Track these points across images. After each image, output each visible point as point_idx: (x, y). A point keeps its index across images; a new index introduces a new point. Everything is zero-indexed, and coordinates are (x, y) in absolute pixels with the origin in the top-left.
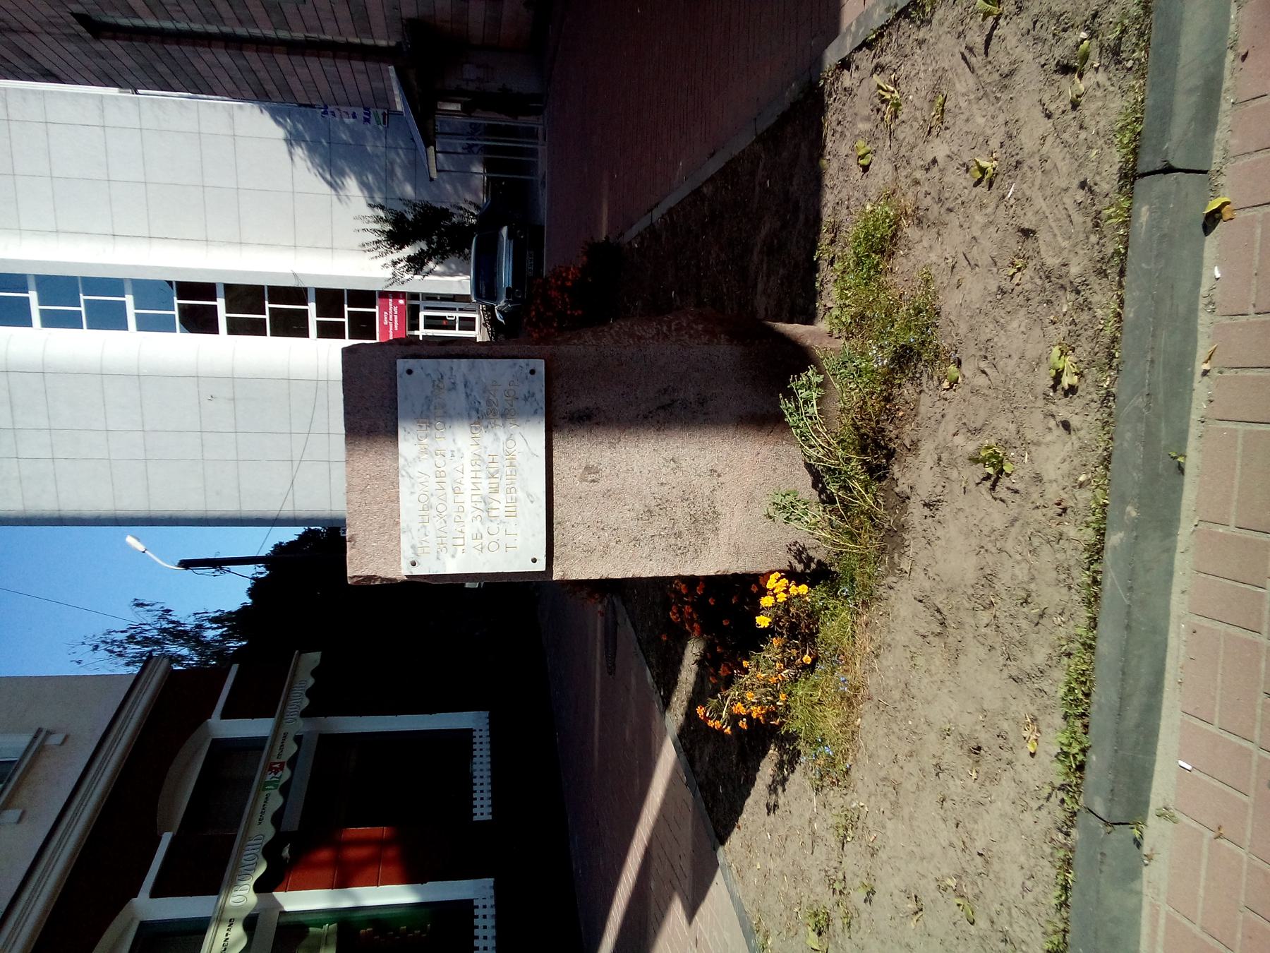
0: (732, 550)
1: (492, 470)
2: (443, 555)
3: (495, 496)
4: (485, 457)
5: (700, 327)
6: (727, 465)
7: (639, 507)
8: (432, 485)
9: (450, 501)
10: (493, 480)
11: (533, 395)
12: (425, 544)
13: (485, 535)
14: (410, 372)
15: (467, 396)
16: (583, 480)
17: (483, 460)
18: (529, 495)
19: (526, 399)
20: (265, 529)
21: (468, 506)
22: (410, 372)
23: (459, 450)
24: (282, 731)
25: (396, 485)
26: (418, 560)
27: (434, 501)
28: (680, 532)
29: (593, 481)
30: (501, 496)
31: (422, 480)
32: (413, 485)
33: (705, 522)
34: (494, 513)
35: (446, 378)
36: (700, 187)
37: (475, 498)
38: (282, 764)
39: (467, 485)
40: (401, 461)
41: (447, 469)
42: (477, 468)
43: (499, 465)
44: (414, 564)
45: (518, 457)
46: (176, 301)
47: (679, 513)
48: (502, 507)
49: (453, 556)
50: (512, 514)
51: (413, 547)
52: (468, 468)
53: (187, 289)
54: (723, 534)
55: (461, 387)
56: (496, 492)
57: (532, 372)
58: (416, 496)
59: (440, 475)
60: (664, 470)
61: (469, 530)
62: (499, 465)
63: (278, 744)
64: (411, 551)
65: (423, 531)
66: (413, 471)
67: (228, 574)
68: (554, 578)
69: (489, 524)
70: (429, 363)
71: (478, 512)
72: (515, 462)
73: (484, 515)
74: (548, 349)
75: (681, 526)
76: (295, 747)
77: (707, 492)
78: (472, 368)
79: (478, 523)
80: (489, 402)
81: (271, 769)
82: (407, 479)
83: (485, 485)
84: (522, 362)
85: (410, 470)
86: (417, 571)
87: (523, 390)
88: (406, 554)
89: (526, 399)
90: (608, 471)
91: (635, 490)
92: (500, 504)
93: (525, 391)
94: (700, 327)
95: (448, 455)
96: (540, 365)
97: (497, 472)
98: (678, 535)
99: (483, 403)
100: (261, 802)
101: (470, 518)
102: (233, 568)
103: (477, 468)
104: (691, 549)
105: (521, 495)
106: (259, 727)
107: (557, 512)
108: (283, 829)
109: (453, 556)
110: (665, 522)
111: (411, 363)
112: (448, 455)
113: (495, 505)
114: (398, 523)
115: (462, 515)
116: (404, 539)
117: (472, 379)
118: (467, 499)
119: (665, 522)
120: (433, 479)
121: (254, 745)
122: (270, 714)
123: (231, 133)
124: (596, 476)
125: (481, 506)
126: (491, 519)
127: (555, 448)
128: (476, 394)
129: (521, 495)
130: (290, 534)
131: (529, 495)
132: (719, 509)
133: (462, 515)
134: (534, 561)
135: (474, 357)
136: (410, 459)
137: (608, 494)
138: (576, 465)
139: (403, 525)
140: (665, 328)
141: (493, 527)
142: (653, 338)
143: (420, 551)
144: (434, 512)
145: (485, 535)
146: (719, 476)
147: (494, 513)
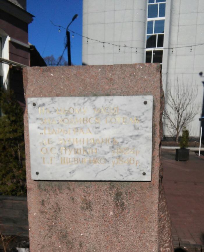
2: (39, 122)
3: (73, 152)
10: (82, 151)
11: (131, 174)
18: (73, 171)
19: (129, 170)
23: (99, 132)
25: (80, 95)
26: (36, 107)
27: (70, 116)
35: (142, 124)
39: (80, 136)
44: (34, 105)
46: (157, 34)
49: (39, 128)
51: (44, 105)
53: (161, 38)
55: (136, 133)
57: (144, 174)
58: (73, 106)
65: (53, 110)
66: (88, 104)
67: (64, 48)
69: (57, 148)
87: (134, 168)
88: (39, 101)
89: (129, 170)
95: (97, 125)
97: (88, 153)
102: (66, 51)
105: (74, 166)
109: (39, 128)
113: (68, 151)
118: (72, 137)
131: (73, 171)
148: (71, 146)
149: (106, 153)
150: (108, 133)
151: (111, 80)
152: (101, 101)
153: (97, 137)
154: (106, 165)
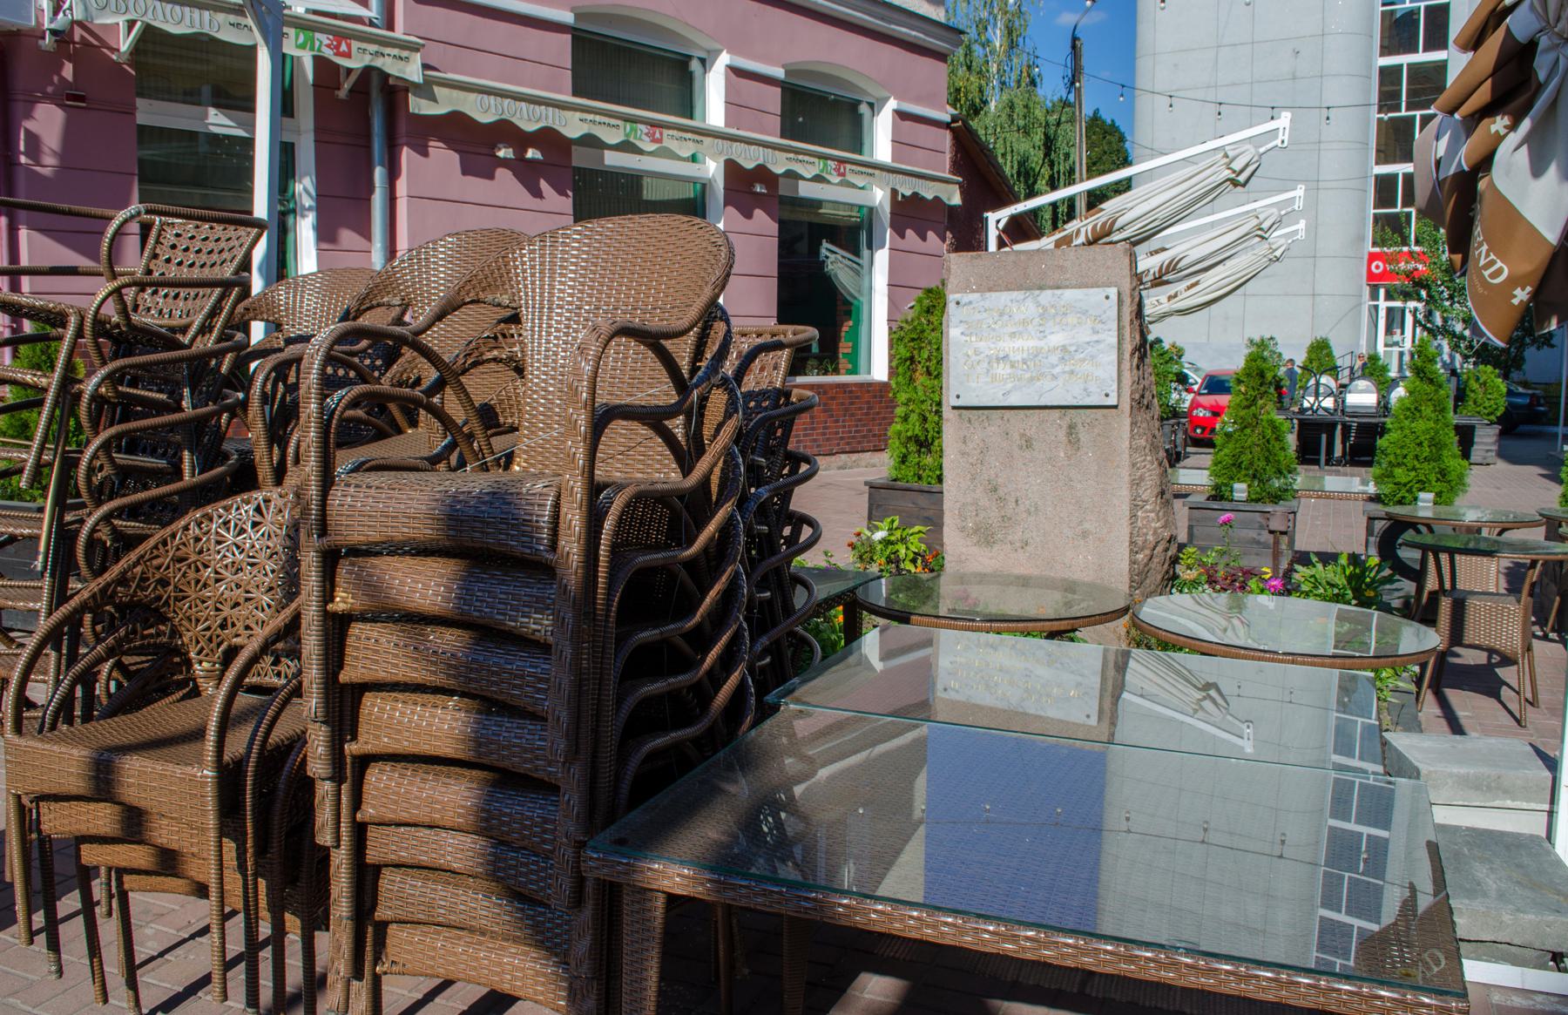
21: (1001, 344)
25: (1020, 288)
27: (1006, 317)
39: (1019, 343)
41: (1030, 327)
50: (994, 378)
54: (975, 550)
55: (1095, 338)
56: (1012, 366)
59: (1024, 322)
66: (1030, 303)
68: (1555, 243)
74: (1126, 405)
76: (687, 154)
80: (1083, 360)
84: (1115, 386)
86: (951, 306)
87: (1093, 388)
92: (1002, 370)
96: (1112, 401)
105: (1009, 386)
108: (781, 180)
111: (1114, 297)
116: (976, 296)
117: (1101, 346)
118: (1007, 345)
123: (1318, 299)
127: (458, 632)
132: (996, 547)
148: (1006, 357)
149: (1054, 366)
150: (1057, 339)
151: (1062, 267)
152: (1046, 296)
153: (1041, 344)
154: (1054, 384)
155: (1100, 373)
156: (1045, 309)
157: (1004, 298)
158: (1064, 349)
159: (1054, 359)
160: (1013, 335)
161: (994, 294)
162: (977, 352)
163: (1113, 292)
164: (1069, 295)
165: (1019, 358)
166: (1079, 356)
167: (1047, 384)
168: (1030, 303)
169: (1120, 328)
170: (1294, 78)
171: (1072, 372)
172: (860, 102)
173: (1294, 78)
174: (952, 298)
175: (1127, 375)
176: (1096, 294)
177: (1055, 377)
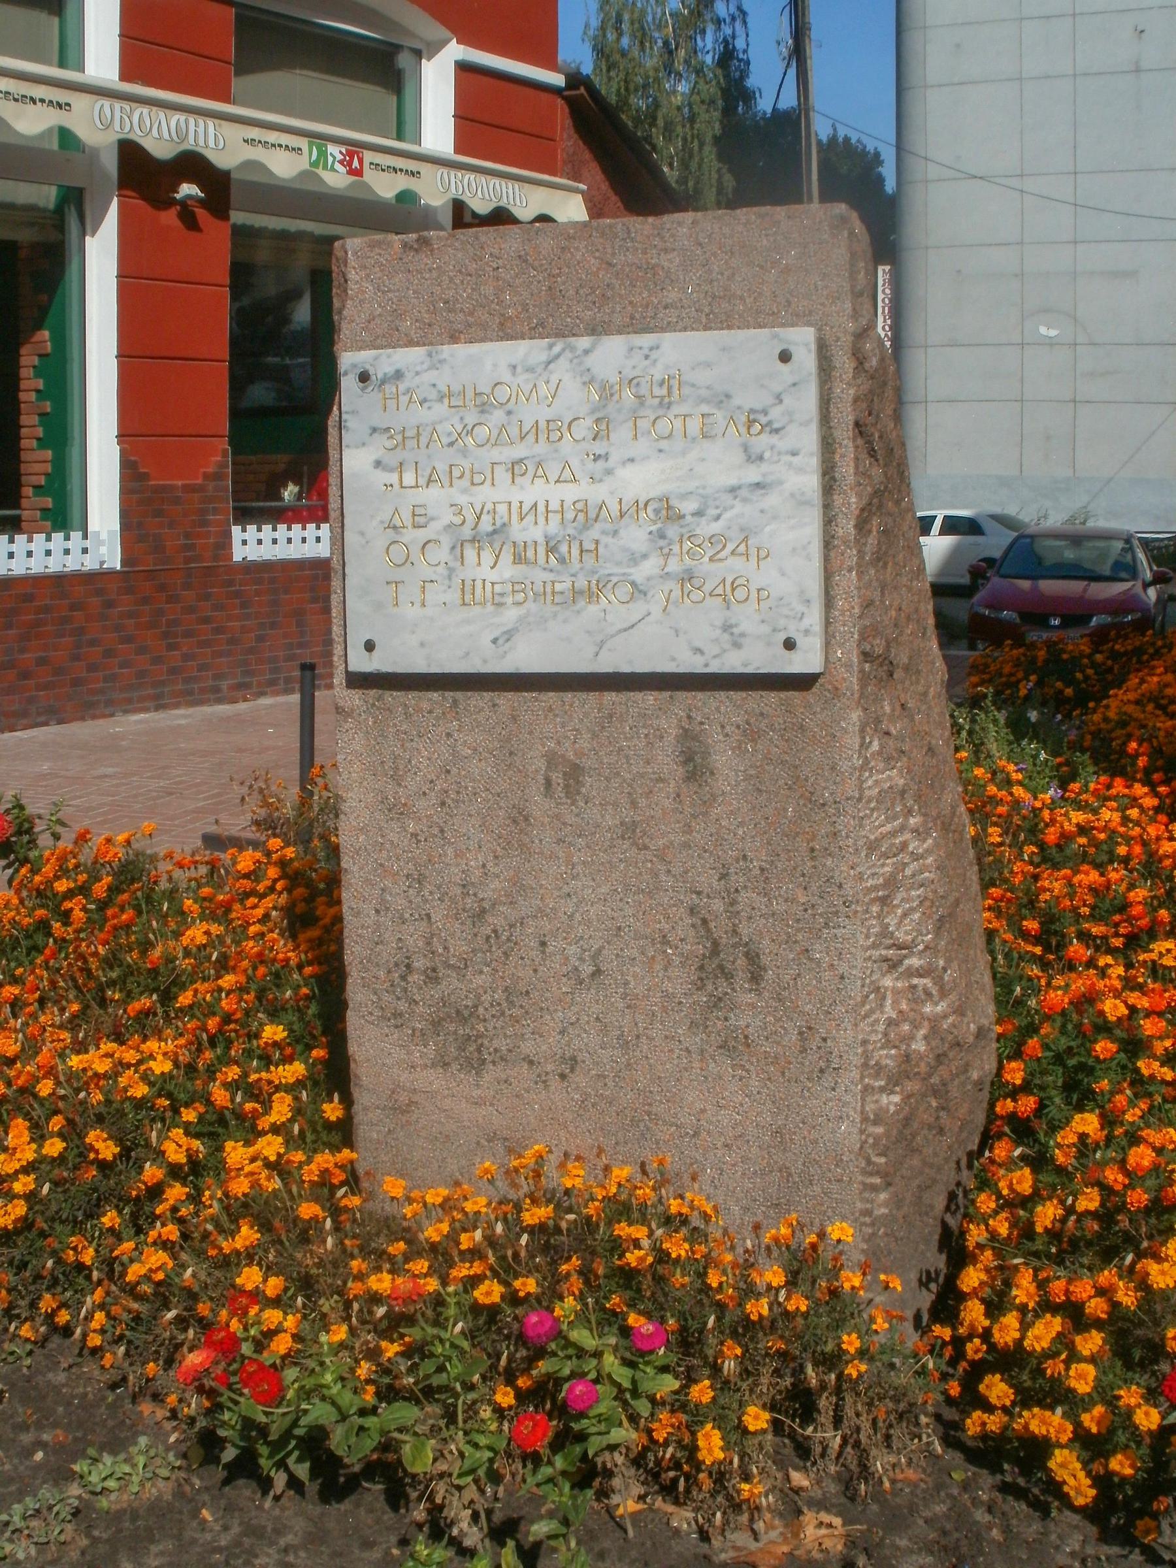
0: (403, 1098)
1: (564, 549)
2: (382, 440)
3: (507, 557)
4: (594, 533)
5: (919, 1046)
6: (586, 1097)
7: (492, 889)
8: (531, 413)
9: (496, 454)
10: (541, 550)
11: (737, 645)
12: (404, 399)
13: (422, 535)
14: (785, 357)
15: (733, 490)
16: (552, 760)
17: (586, 527)
18: (509, 635)
20: (893, 139)
21: (485, 494)
22: (785, 357)
24: (425, 168)
25: (537, 331)
27: (498, 416)
28: (436, 980)
29: (548, 783)
30: (507, 570)
31: (543, 389)
32: (530, 370)
33: (464, 1040)
34: (470, 553)
35: (774, 439)
36: (347, 1101)
37: (502, 509)
38: (358, 173)
39: (533, 492)
40: (584, 342)
42: (570, 515)
43: (576, 565)
44: (364, 377)
45: (593, 608)
47: (479, 981)
48: (485, 572)
50: (468, 594)
51: (398, 375)
52: (570, 493)
54: (433, 1079)
55: (753, 474)
56: (518, 559)
58: (506, 376)
59: (551, 431)
60: (572, 950)
61: (434, 497)
62: (576, 565)
63: (400, 163)
64: (390, 370)
65: (433, 395)
66: (562, 370)
69: (446, 541)
70: (807, 402)
71: (471, 518)
72: (581, 603)
73: (467, 532)
75: (451, 983)
77: (527, 1047)
78: (802, 502)
79: (448, 517)
81: (351, 154)
82: (544, 357)
83: (531, 532)
84: (814, 618)
85: (563, 363)
86: (348, 385)
87: (748, 619)
88: (384, 361)
89: (727, 628)
90: (571, 819)
91: (529, 881)
92: (490, 570)
93: (746, 626)
94: (919, 1046)
95: (599, 448)
97: (562, 561)
98: (432, 976)
99: (716, 527)
100: (285, 139)
101: (462, 500)
103: (570, 515)
104: (403, 1006)
105: (511, 615)
106: (437, 128)
107: (478, 700)
109: (378, 464)
110: (459, 947)
111: (806, 360)
112: (599, 448)
114: (454, 339)
115: (465, 482)
116: (418, 353)
117: (772, 500)
118: (501, 493)
119: (459, 947)
120: (543, 414)
121: (404, 124)
122: (461, 146)
124: (559, 792)
125: (486, 525)
126: (458, 547)
128: (738, 510)
129: (511, 615)
130: (890, 186)
131: (509, 635)
132: (490, 1074)
133: (465, 482)
134: (370, 646)
135: (827, 506)
136: (590, 361)
137: (520, 818)
138: (584, 743)
139: (446, 350)
140: (915, 962)
141: (441, 554)
142: (885, 933)
143: (390, 389)
144: (471, 419)
145: (422, 535)
146: (563, 1076)
147: (470, 553)
149: (635, 559)
150: (641, 477)
152: (611, 354)
153: (597, 493)
154: (637, 609)
155: (768, 580)
156: (607, 392)
157: (491, 361)
158: (667, 511)
159: (636, 536)
160: (515, 468)
161: (461, 351)
162: (420, 518)
163: (802, 339)
164: (677, 350)
165: (536, 533)
166: (706, 528)
167: (614, 610)
168: (562, 370)
169: (828, 445)
170: (1138, 70)
171: (687, 577)
172: (398, 48)
173: (1138, 70)
174: (349, 360)
175: (848, 581)
176: (752, 346)
177: (639, 591)
